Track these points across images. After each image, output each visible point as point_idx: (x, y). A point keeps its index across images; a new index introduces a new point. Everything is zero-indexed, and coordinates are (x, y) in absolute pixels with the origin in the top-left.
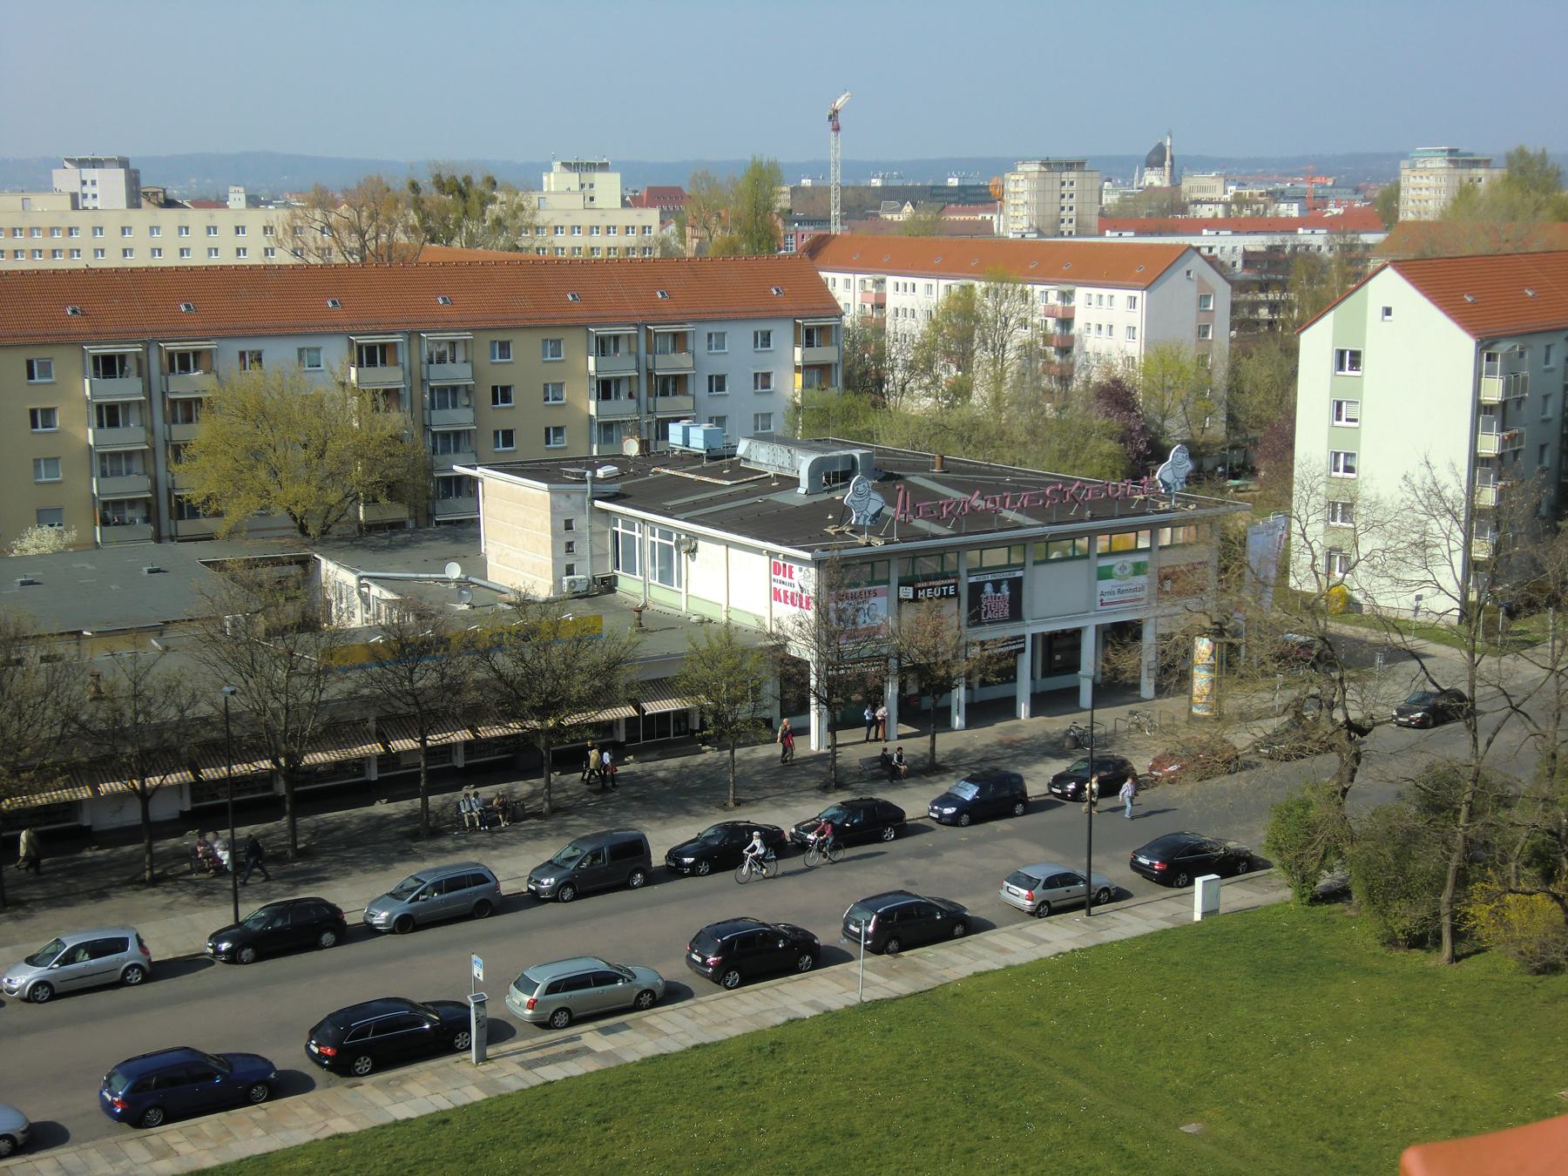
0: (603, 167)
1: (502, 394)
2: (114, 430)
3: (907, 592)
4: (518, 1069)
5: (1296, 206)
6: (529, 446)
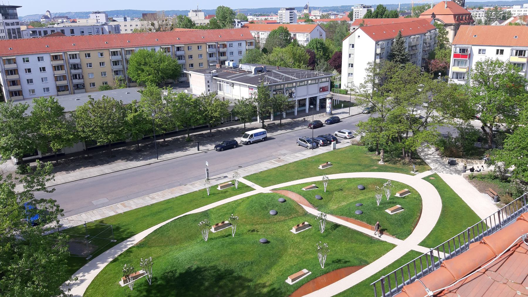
0: (200, 11)
1: (191, 57)
2: (116, 66)
3: (275, 93)
4: (215, 181)
5: (333, 16)
6: (196, 66)
